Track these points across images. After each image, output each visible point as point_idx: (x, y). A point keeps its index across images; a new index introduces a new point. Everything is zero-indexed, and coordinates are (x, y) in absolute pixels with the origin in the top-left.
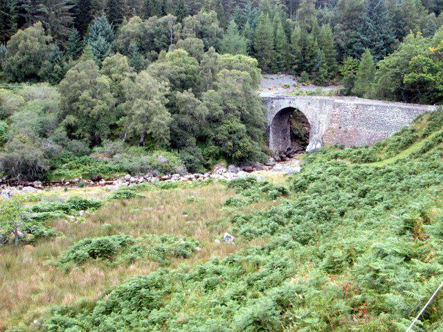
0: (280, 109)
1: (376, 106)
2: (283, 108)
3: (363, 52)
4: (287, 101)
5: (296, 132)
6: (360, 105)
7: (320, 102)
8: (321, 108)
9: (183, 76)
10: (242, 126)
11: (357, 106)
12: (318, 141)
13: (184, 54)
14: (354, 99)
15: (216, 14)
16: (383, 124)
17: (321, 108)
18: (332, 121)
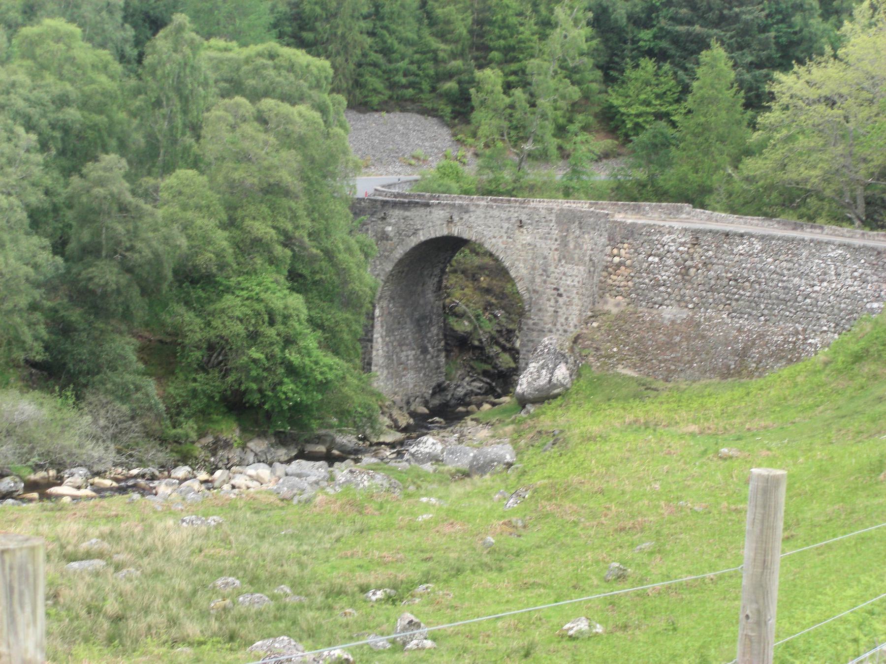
0: (414, 242)
1: (762, 238)
2: (422, 237)
3: (703, 44)
4: (438, 215)
5: (463, 326)
6: (705, 232)
7: (559, 222)
8: (564, 242)
9: (72, 114)
10: (296, 301)
11: (697, 237)
12: (560, 357)
13: (71, 35)
14: (679, 211)
15: (620, 366)
16: (789, 298)
17: (564, 242)
18: (604, 289)
